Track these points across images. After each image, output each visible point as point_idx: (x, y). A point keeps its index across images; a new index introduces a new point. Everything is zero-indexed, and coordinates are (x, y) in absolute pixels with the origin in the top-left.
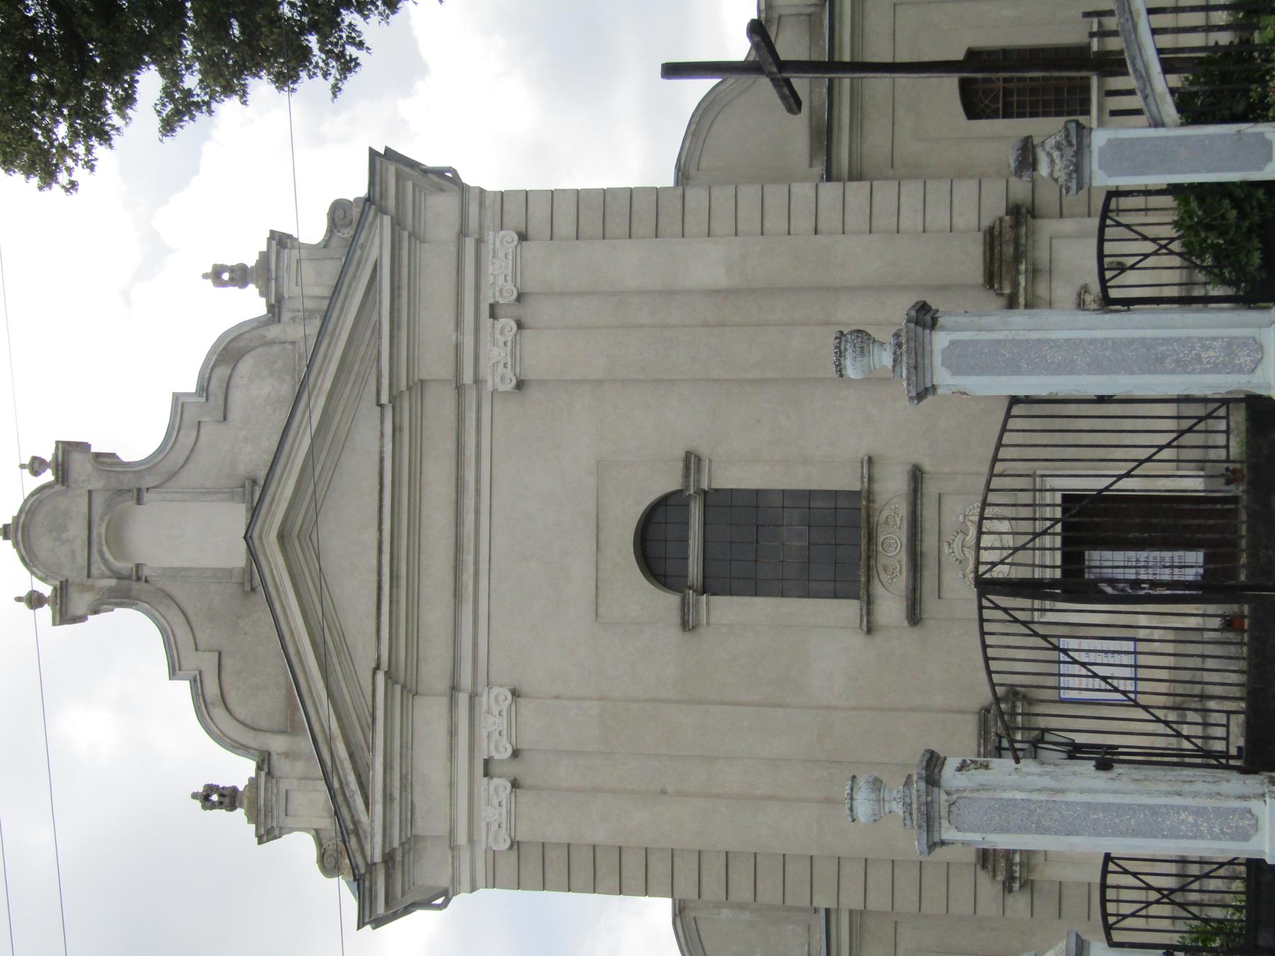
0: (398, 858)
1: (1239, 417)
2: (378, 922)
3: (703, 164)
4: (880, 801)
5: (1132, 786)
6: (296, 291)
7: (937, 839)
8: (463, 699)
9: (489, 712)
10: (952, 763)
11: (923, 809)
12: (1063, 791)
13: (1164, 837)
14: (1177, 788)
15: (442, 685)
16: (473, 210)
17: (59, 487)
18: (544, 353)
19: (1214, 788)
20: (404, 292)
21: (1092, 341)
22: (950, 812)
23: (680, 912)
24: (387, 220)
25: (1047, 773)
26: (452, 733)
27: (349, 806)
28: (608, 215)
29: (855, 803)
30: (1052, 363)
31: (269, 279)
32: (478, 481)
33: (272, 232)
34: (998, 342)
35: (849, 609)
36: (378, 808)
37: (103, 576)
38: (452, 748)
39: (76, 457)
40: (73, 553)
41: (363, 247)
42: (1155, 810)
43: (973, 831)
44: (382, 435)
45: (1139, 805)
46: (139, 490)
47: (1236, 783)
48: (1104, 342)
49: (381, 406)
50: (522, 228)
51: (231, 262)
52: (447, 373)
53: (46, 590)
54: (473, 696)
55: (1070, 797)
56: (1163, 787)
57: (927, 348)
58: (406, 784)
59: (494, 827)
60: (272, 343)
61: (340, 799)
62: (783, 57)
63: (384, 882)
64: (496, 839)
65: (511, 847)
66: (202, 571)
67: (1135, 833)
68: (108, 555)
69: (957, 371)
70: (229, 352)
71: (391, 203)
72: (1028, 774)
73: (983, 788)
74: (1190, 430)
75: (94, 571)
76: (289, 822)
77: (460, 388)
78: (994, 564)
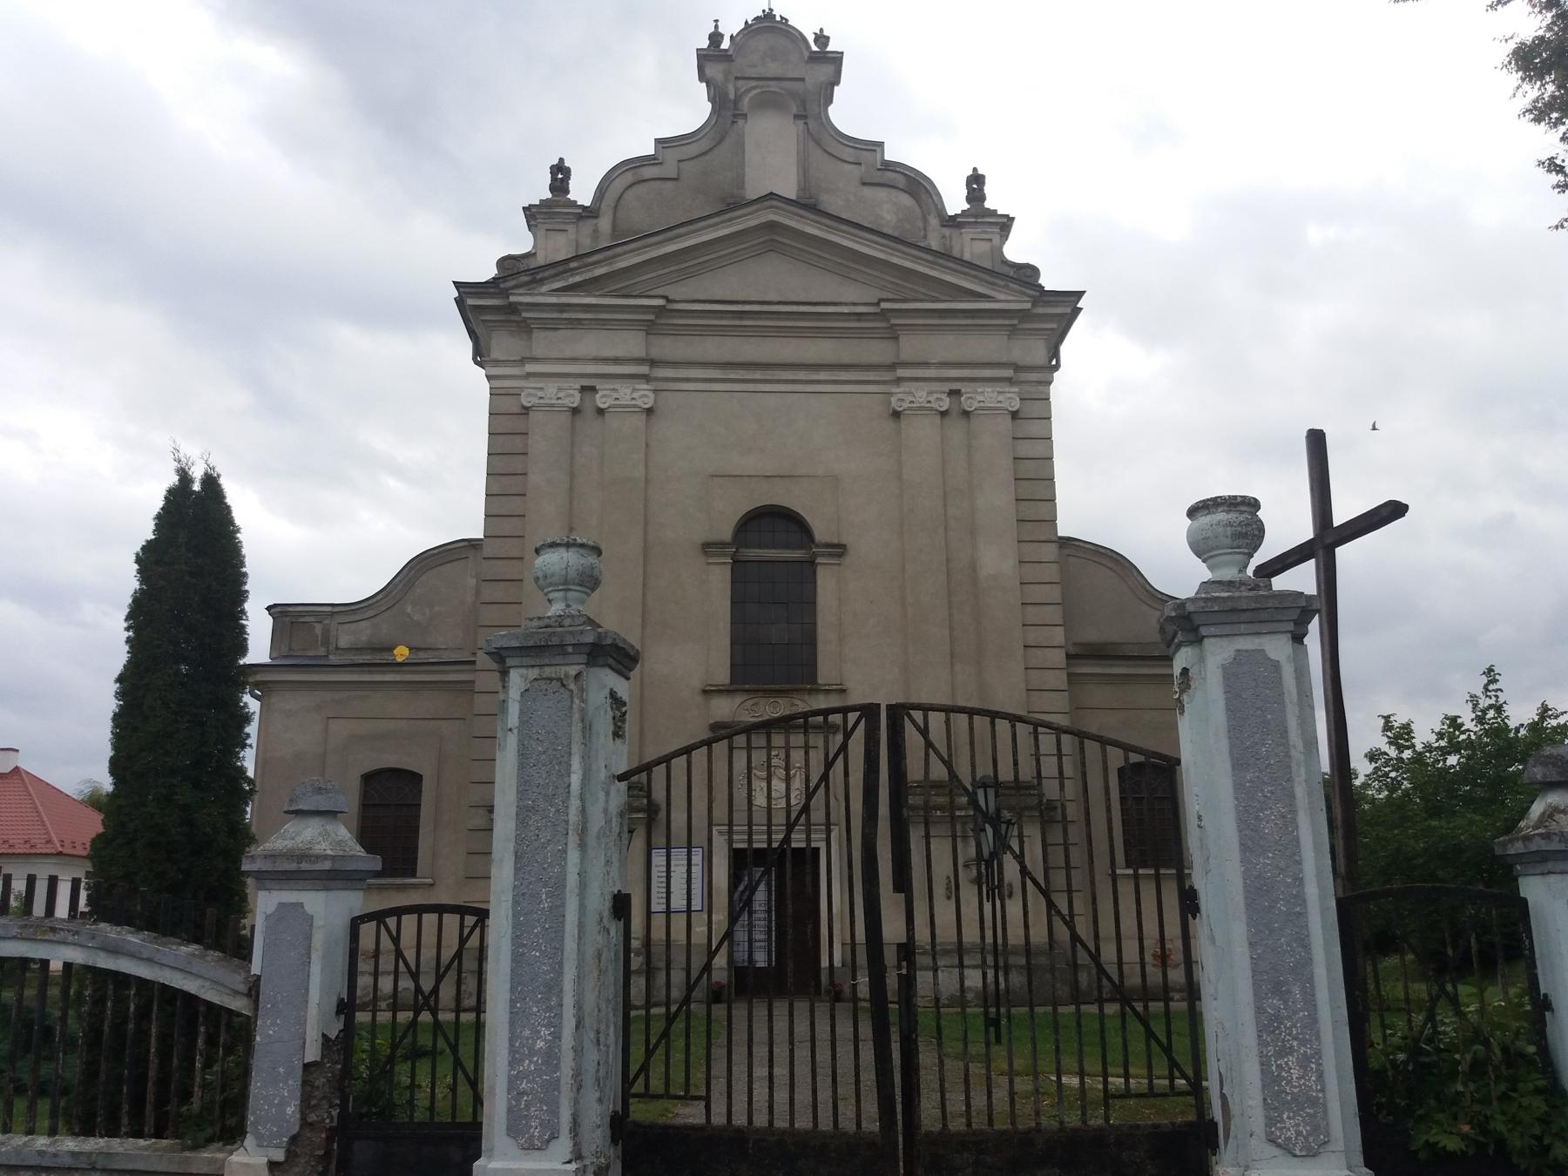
0: (513, 318)
1: (1179, 1113)
2: (459, 302)
3: (1072, 560)
4: (565, 584)
5: (590, 951)
6: (967, 238)
7: (510, 662)
8: (644, 369)
9: (634, 390)
10: (623, 688)
11: (555, 641)
12: (582, 846)
13: (513, 1002)
14: (587, 1021)
15: (655, 353)
16: (1034, 376)
17: (806, 54)
18: (922, 432)
19: (589, 1079)
20: (969, 322)
21: (1299, 881)
22: (551, 679)
23: (471, 544)
24: (1028, 306)
25: (608, 822)
26: (617, 361)
27: (556, 275)
28: (1034, 482)
29: (562, 550)
30: (1257, 818)
31: (976, 216)
32: (818, 382)
33: (1013, 219)
34: (1284, 733)
35: (722, 676)
36: (553, 300)
37: (736, 89)
38: (606, 360)
39: (830, 68)
40: (754, 66)
41: (1006, 286)
42: (554, 987)
43: (522, 712)
44: (855, 304)
45: (561, 964)
46: (805, 117)
47: (596, 1114)
48: (1300, 899)
49: (878, 304)
50: (1021, 415)
51: (987, 189)
52: (905, 356)
53: (725, 45)
54: (646, 378)
55: (573, 856)
56: (590, 998)
57: (1264, 628)
58: (575, 324)
59: (540, 394)
60: (925, 221)
61: (561, 268)
62: (1338, 550)
63: (491, 309)
64: (529, 395)
65: (524, 408)
66: (742, 166)
67: (517, 958)
68: (754, 92)
69: (1231, 674)
70: (917, 186)
71: (1041, 310)
72: (607, 794)
73: (587, 728)
74: (1150, 1034)
75: (740, 83)
76: (541, 233)
77: (893, 366)
78: (924, 732)
